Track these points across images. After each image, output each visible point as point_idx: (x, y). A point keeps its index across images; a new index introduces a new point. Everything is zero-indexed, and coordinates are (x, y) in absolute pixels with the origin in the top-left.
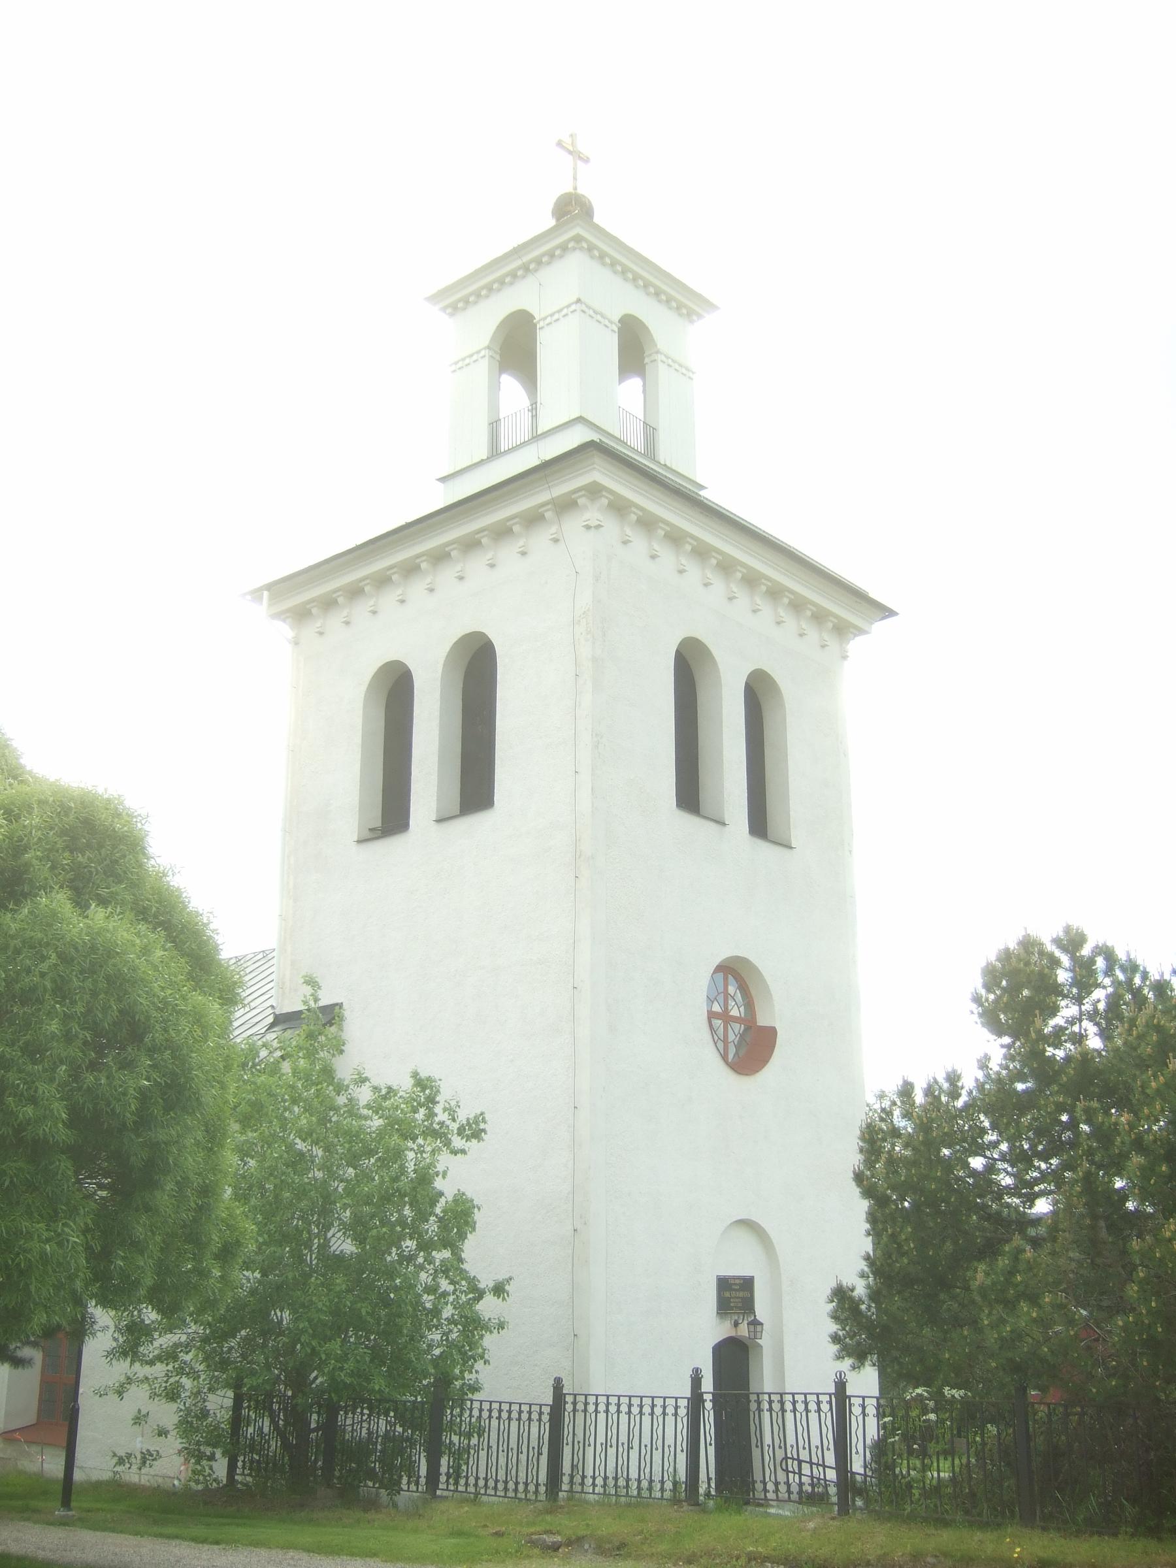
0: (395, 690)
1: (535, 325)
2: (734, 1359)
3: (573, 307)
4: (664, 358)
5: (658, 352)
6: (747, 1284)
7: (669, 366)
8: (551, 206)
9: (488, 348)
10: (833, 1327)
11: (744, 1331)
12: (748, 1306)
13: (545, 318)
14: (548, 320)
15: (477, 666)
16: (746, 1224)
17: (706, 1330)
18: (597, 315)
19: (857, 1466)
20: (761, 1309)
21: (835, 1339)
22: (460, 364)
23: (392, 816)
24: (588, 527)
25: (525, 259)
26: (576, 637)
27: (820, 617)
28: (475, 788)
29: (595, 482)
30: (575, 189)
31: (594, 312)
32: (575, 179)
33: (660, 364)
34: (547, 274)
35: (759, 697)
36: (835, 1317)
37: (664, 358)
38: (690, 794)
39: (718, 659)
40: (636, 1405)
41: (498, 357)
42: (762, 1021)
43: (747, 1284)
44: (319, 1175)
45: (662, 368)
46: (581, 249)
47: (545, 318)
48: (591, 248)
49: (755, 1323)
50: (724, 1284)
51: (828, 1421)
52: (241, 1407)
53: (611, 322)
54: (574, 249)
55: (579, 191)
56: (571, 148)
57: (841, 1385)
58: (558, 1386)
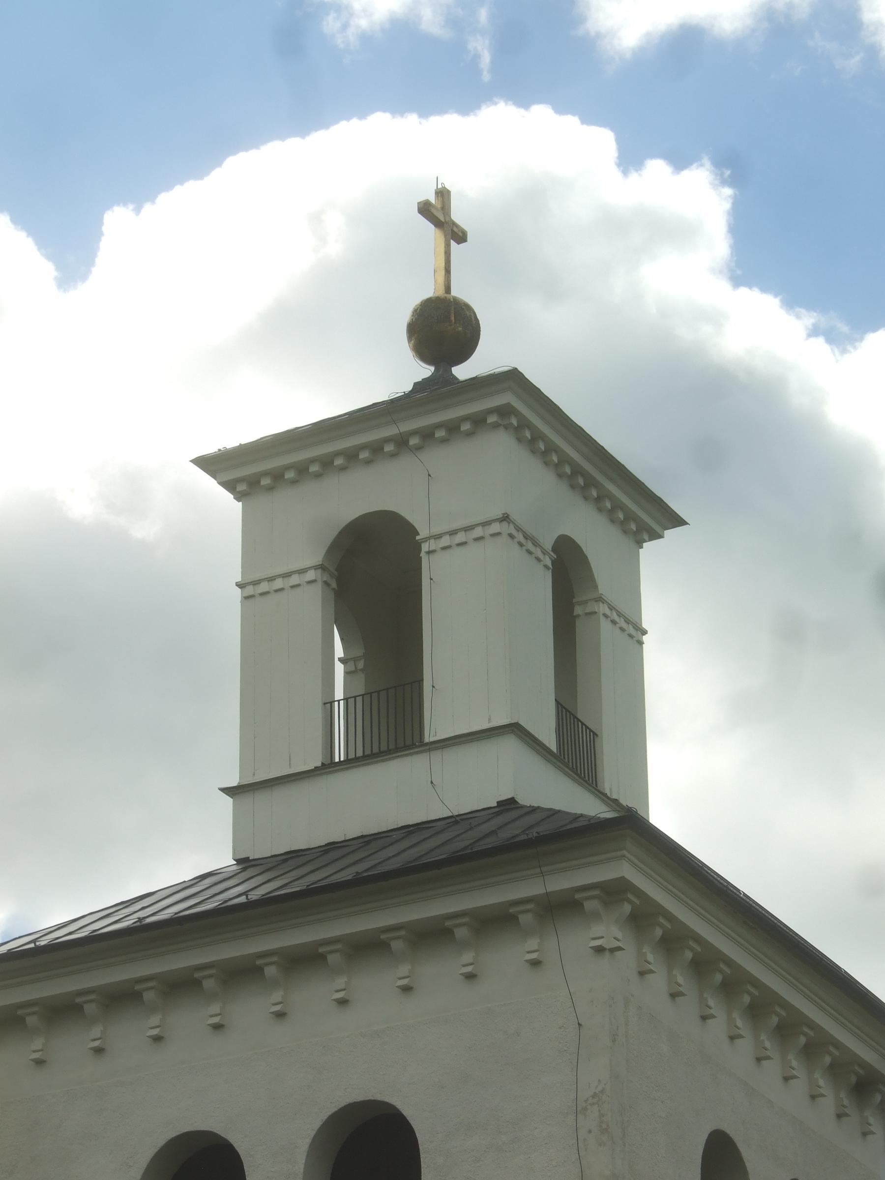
1: (418, 547)
3: (495, 528)
4: (608, 612)
5: (600, 599)
7: (614, 622)
8: (405, 316)
9: (321, 567)
13: (438, 537)
14: (445, 541)
18: (527, 540)
22: (264, 587)
24: (599, 950)
25: (406, 426)
29: (623, 879)
30: (448, 289)
31: (526, 537)
32: (448, 271)
33: (605, 625)
34: (442, 460)
37: (608, 612)
39: (749, 1166)
41: (334, 585)
46: (506, 427)
47: (438, 537)
48: (524, 424)
53: (544, 552)
54: (496, 426)
56: (441, 218)
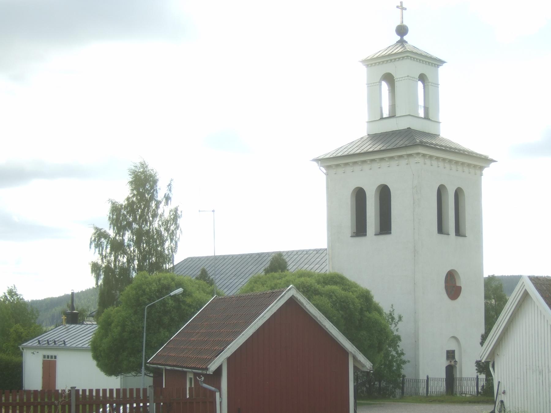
0: (360, 196)
2: (450, 370)
6: (453, 352)
10: (476, 368)
11: (453, 363)
12: (454, 357)
15: (384, 194)
16: (454, 337)
17: (444, 363)
19: (480, 391)
20: (457, 357)
21: (477, 370)
23: (360, 230)
26: (411, 183)
27: (475, 166)
28: (385, 227)
35: (458, 194)
36: (476, 366)
38: (441, 230)
40: (467, 379)
42: (458, 285)
43: (453, 352)
44: (128, 235)
45: (430, 87)
49: (456, 361)
50: (448, 352)
51: (475, 382)
52: (486, 380)
55: (405, 23)
57: (477, 377)
58: (428, 377)
